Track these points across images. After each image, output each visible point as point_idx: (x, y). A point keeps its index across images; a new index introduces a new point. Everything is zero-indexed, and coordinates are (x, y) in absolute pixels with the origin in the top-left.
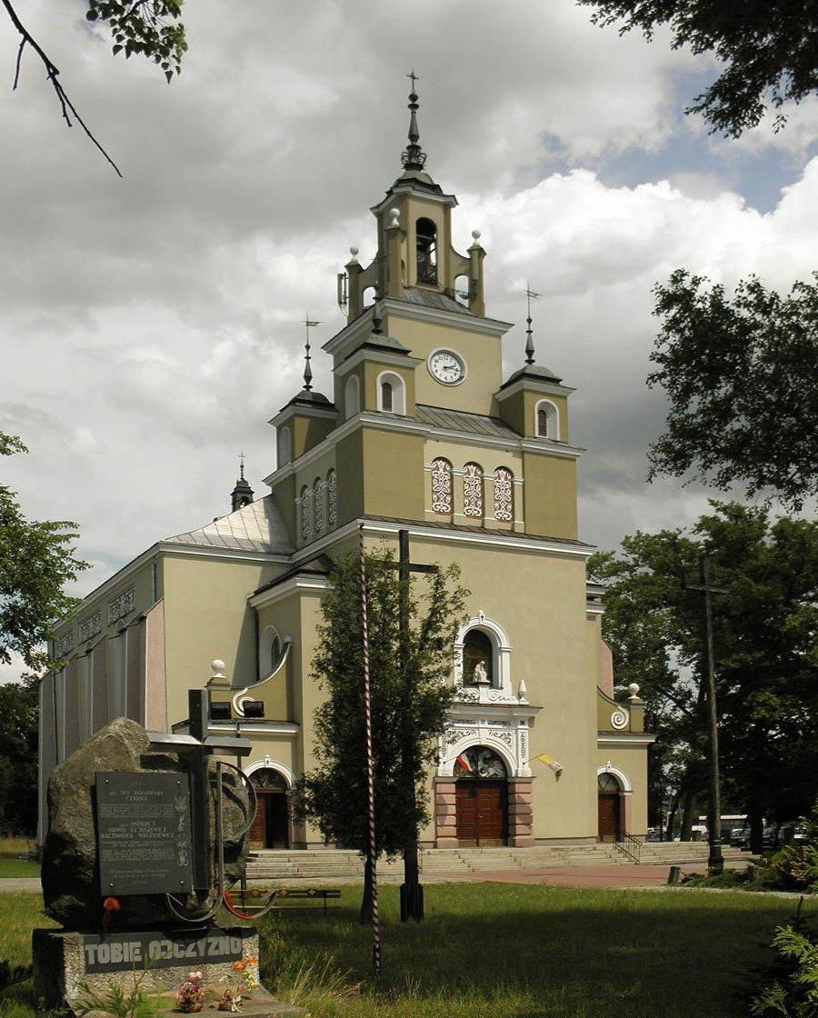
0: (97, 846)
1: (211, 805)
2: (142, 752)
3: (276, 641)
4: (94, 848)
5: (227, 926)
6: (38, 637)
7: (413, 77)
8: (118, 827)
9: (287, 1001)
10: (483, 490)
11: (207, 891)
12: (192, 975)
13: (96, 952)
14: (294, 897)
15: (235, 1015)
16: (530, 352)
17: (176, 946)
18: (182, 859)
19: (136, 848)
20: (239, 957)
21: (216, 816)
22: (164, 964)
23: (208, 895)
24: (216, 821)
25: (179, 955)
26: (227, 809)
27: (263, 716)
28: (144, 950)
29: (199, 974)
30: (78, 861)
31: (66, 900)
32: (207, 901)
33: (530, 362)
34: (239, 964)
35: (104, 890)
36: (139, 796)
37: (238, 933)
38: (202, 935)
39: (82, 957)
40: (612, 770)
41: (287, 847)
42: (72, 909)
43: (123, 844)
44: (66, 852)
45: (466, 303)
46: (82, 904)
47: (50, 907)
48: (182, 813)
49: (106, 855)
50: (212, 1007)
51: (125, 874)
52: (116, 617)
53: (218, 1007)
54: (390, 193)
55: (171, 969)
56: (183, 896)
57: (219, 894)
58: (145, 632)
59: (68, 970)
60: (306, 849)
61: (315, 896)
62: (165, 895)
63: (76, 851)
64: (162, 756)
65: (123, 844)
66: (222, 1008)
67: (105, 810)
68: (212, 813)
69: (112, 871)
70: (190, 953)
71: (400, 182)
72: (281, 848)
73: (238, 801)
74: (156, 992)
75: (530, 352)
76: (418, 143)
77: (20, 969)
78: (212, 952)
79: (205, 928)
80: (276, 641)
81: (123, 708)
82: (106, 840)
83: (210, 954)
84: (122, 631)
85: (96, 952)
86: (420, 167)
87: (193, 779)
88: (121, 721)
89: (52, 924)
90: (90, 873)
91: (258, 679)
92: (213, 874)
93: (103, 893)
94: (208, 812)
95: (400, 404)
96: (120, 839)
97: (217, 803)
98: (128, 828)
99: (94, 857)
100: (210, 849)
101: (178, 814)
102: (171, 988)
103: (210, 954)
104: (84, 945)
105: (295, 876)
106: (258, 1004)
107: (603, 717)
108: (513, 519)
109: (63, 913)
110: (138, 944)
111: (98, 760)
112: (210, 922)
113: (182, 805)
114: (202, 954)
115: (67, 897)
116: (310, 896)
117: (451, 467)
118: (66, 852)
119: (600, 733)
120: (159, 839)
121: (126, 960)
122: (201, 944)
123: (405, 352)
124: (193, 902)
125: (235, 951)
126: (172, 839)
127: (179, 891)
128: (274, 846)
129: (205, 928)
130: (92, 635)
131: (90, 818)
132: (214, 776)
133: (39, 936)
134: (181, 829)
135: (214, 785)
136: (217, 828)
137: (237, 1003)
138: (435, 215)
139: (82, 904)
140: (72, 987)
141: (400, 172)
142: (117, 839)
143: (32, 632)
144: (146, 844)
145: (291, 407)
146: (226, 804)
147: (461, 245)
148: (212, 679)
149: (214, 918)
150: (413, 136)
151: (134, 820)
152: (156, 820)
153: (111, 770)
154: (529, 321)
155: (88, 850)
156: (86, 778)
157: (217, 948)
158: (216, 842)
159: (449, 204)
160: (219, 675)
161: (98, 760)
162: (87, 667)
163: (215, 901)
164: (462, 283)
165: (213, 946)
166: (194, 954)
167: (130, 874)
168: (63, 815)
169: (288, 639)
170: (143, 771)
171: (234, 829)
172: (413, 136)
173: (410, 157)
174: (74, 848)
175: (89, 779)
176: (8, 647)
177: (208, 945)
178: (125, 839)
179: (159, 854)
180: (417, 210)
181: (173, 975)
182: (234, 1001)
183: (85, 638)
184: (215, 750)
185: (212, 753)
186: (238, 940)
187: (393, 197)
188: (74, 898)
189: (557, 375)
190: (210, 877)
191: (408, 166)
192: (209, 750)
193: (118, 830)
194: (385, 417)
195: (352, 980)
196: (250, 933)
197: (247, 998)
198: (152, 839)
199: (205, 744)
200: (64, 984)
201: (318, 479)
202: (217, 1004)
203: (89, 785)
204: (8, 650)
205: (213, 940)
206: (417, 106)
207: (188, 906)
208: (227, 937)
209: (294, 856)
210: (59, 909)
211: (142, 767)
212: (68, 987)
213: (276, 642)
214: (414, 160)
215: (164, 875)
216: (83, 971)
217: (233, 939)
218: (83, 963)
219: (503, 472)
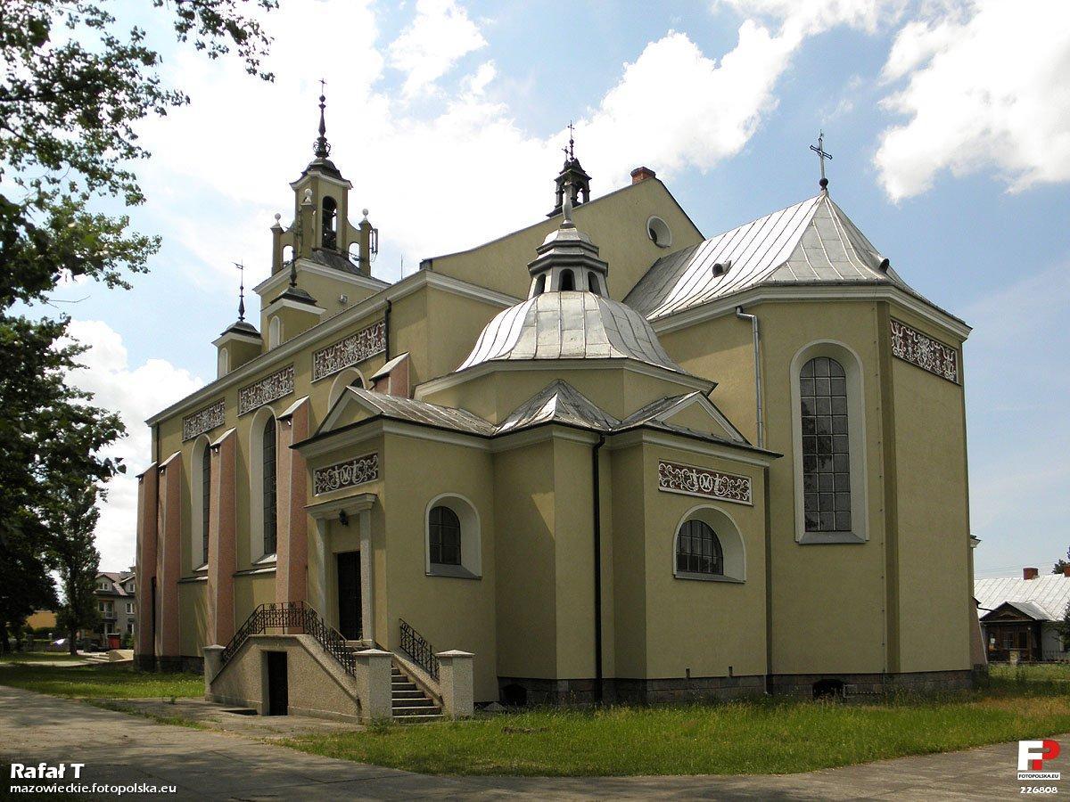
150: (322, 130)
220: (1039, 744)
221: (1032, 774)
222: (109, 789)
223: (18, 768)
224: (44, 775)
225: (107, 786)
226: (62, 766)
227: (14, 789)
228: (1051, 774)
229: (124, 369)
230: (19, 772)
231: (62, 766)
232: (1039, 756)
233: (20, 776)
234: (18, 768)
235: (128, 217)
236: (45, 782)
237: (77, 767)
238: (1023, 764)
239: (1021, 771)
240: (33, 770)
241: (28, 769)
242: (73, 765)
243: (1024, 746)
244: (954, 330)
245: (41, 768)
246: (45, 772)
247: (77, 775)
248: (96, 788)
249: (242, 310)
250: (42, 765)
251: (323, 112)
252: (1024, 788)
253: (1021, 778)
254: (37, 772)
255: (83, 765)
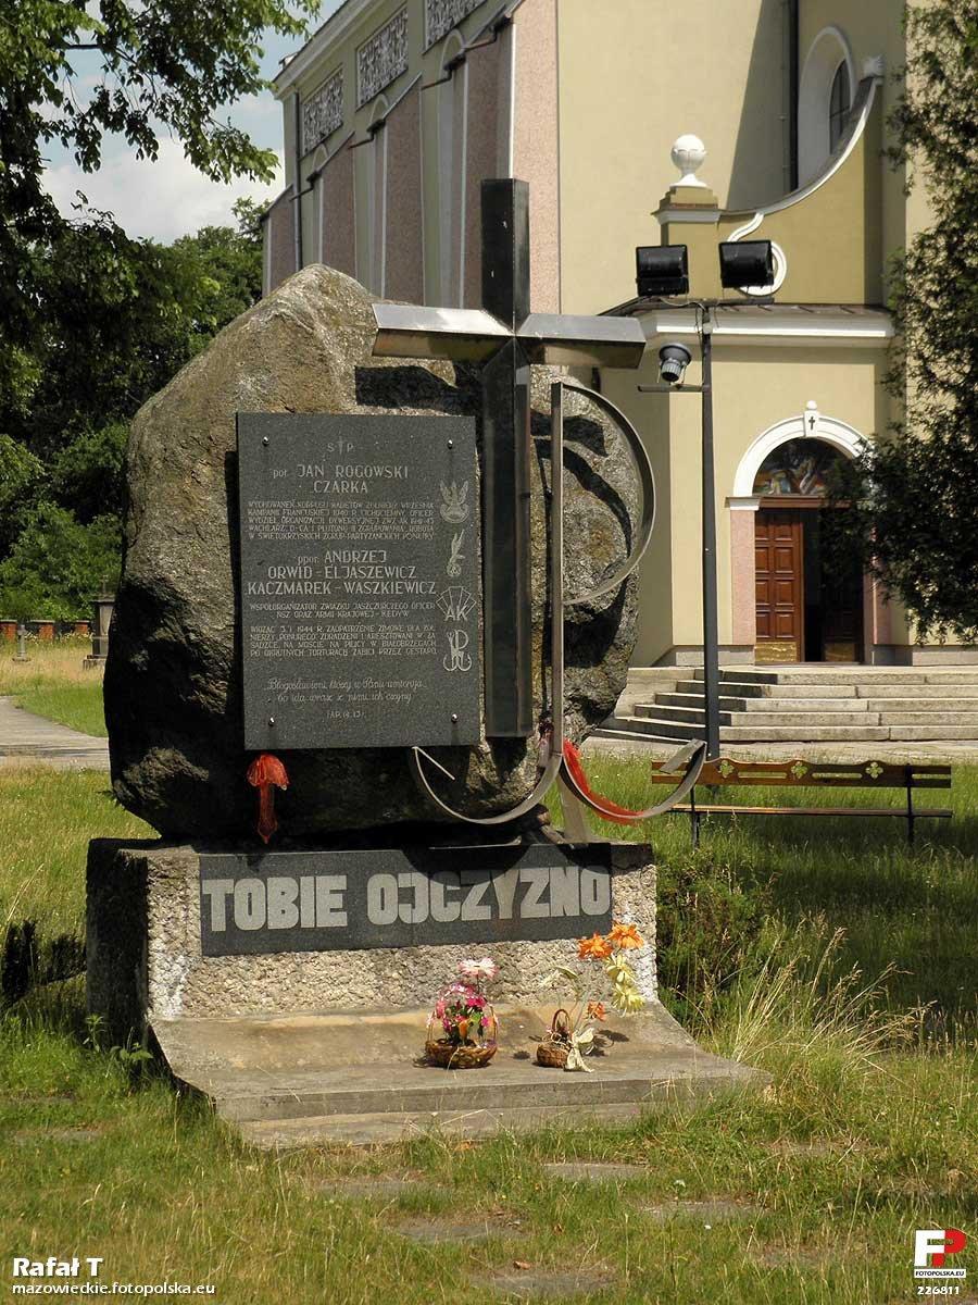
0: (238, 617)
1: (536, 507)
2: (361, 358)
3: (842, 71)
4: (230, 620)
5: (573, 840)
6: (224, 83)
8: (294, 564)
9: (727, 1050)
11: (523, 740)
12: (470, 966)
13: (230, 899)
14: (827, 781)
15: (572, 1078)
17: (438, 888)
19: (336, 621)
20: (603, 924)
21: (549, 535)
22: (406, 937)
23: (522, 754)
24: (549, 551)
25: (446, 913)
26: (578, 517)
27: (766, 279)
28: (354, 900)
29: (487, 965)
30: (187, 658)
31: (163, 760)
32: (521, 771)
34: (598, 944)
35: (254, 738)
36: (348, 480)
37: (599, 857)
38: (504, 861)
39: (195, 911)
41: (860, 659)
42: (176, 785)
43: (303, 611)
44: (161, 634)
46: (202, 773)
47: (124, 780)
48: (457, 528)
49: (259, 640)
50: (522, 1056)
51: (306, 693)
52: (442, 25)
53: (534, 1056)
55: (424, 949)
56: (458, 754)
57: (552, 752)
58: (510, 71)
59: (157, 945)
60: (908, 662)
61: (881, 781)
62: (409, 750)
63: (185, 630)
64: (412, 368)
65: (303, 611)
66: (544, 1061)
67: (259, 517)
68: (538, 528)
69: (274, 684)
70: (472, 908)
72: (841, 661)
73: (609, 495)
74: (380, 1011)
77: (62, 947)
78: (531, 909)
79: (517, 841)
80: (842, 71)
81: (454, 281)
82: (260, 598)
83: (524, 915)
84: (454, 66)
85: (230, 899)
87: (489, 432)
88: (310, 275)
89: (136, 827)
90: (220, 689)
91: (794, 184)
92: (538, 697)
93: (249, 745)
94: (527, 527)
96: (297, 598)
97: (549, 500)
98: (318, 568)
99: (231, 645)
100: (529, 626)
101: (446, 530)
102: (421, 1002)
103: (524, 915)
104: (200, 879)
105: (871, 737)
106: (645, 1054)
109: (153, 794)
110: (341, 882)
111: (247, 383)
112: (530, 825)
113: (460, 505)
114: (505, 913)
115: (165, 754)
116: (867, 781)
118: (161, 634)
120: (399, 599)
121: (307, 923)
122: (504, 885)
124: (484, 773)
125: (595, 909)
126: (430, 598)
127: (446, 741)
128: (828, 654)
129: (517, 841)
130: (385, 83)
131: (222, 541)
132: (543, 424)
133: (105, 860)
134: (453, 570)
135: (545, 450)
136: (550, 571)
137: (582, 1047)
139: (202, 773)
140: (165, 990)
142: (286, 598)
143: (210, 71)
144: (364, 610)
146: (576, 502)
148: (673, 190)
149: (542, 817)
151: (335, 545)
152: (389, 545)
153: (281, 410)
155: (213, 627)
156: (217, 431)
157: (545, 897)
158: (547, 607)
160: (690, 180)
161: (247, 383)
162: (374, 165)
163: (541, 770)
165: (535, 892)
166: (484, 913)
167: (317, 692)
168: (155, 533)
169: (871, 67)
170: (361, 410)
171: (595, 573)
174: (180, 620)
175: (223, 432)
176: (151, 115)
177: (522, 889)
178: (308, 598)
179: (395, 639)
181: (428, 966)
182: (575, 1040)
183: (371, 89)
184: (551, 352)
185: (540, 360)
186: (603, 878)
188: (181, 757)
190: (529, 703)
192: (533, 350)
193: (292, 572)
195: (900, 994)
196: (637, 857)
197: (617, 1037)
198: (380, 598)
199: (523, 333)
200: (147, 981)
202: (532, 1048)
203: (221, 450)
204: (153, 123)
205: (535, 877)
207: (470, 783)
208: (573, 870)
209: (871, 681)
210: (147, 785)
211: (360, 401)
212: (158, 989)
215: (408, 697)
216: (195, 946)
217: (589, 875)
218: (195, 928)
220: (940, 1235)
221: (932, 1270)
222: (132, 1289)
223: (21, 1263)
224: (54, 1272)
225: (130, 1286)
226: (75, 1260)
227: (17, 1289)
228: (955, 1271)
229: (110, 546)
230: (23, 1268)
231: (75, 1261)
232: (940, 1249)
233: (25, 1273)
234: (21, 1263)
235: (87, 168)
236: (62, 1280)
237: (94, 1261)
238: (920, 1259)
239: (917, 1267)
240: (40, 1267)
241: (34, 1264)
242: (89, 1260)
243: (922, 1237)
244: (324, 46)
245: (51, 1263)
246: (55, 1268)
247: (94, 1273)
248: (117, 1288)
250: (51, 1259)
252: (922, 1288)
253: (918, 1276)
254: (45, 1268)
255: (101, 1260)
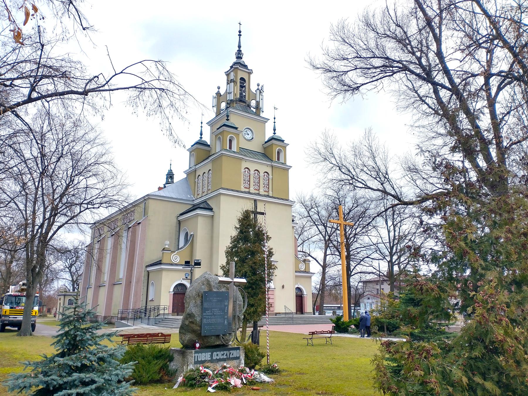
7: (240, 24)
10: (259, 180)
13: (238, 358)
16: (275, 130)
18: (226, 322)
28: (212, 356)
33: (275, 133)
39: (193, 358)
40: (300, 286)
45: (254, 110)
49: (205, 321)
54: (231, 67)
69: (206, 327)
71: (235, 64)
75: (275, 130)
76: (241, 49)
82: (205, 315)
86: (241, 58)
95: (234, 148)
96: (209, 315)
107: (297, 265)
108: (268, 191)
110: (210, 353)
114: (228, 357)
117: (250, 171)
119: (296, 272)
123: (236, 128)
125: (238, 356)
138: (246, 77)
141: (235, 60)
142: (208, 315)
145: (196, 145)
147: (253, 88)
150: (239, 47)
151: (214, 308)
154: (275, 118)
157: (233, 355)
159: (250, 73)
164: (253, 103)
169: (192, 233)
172: (239, 47)
173: (238, 54)
177: (230, 353)
180: (241, 74)
187: (233, 69)
189: (283, 139)
191: (237, 58)
194: (230, 152)
201: (204, 173)
206: (241, 35)
213: (187, 234)
214: (239, 55)
219: (247, 170)
249: (201, 134)
251: (240, 37)
